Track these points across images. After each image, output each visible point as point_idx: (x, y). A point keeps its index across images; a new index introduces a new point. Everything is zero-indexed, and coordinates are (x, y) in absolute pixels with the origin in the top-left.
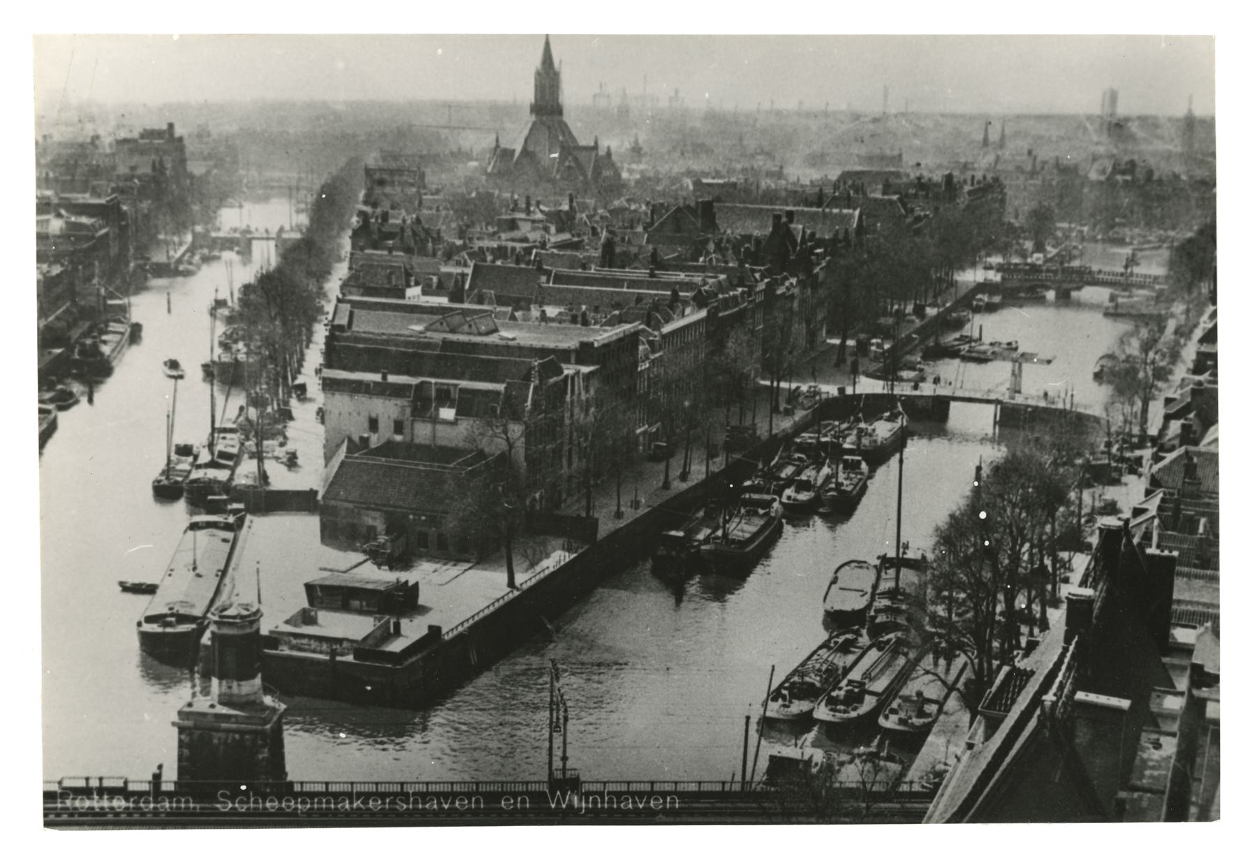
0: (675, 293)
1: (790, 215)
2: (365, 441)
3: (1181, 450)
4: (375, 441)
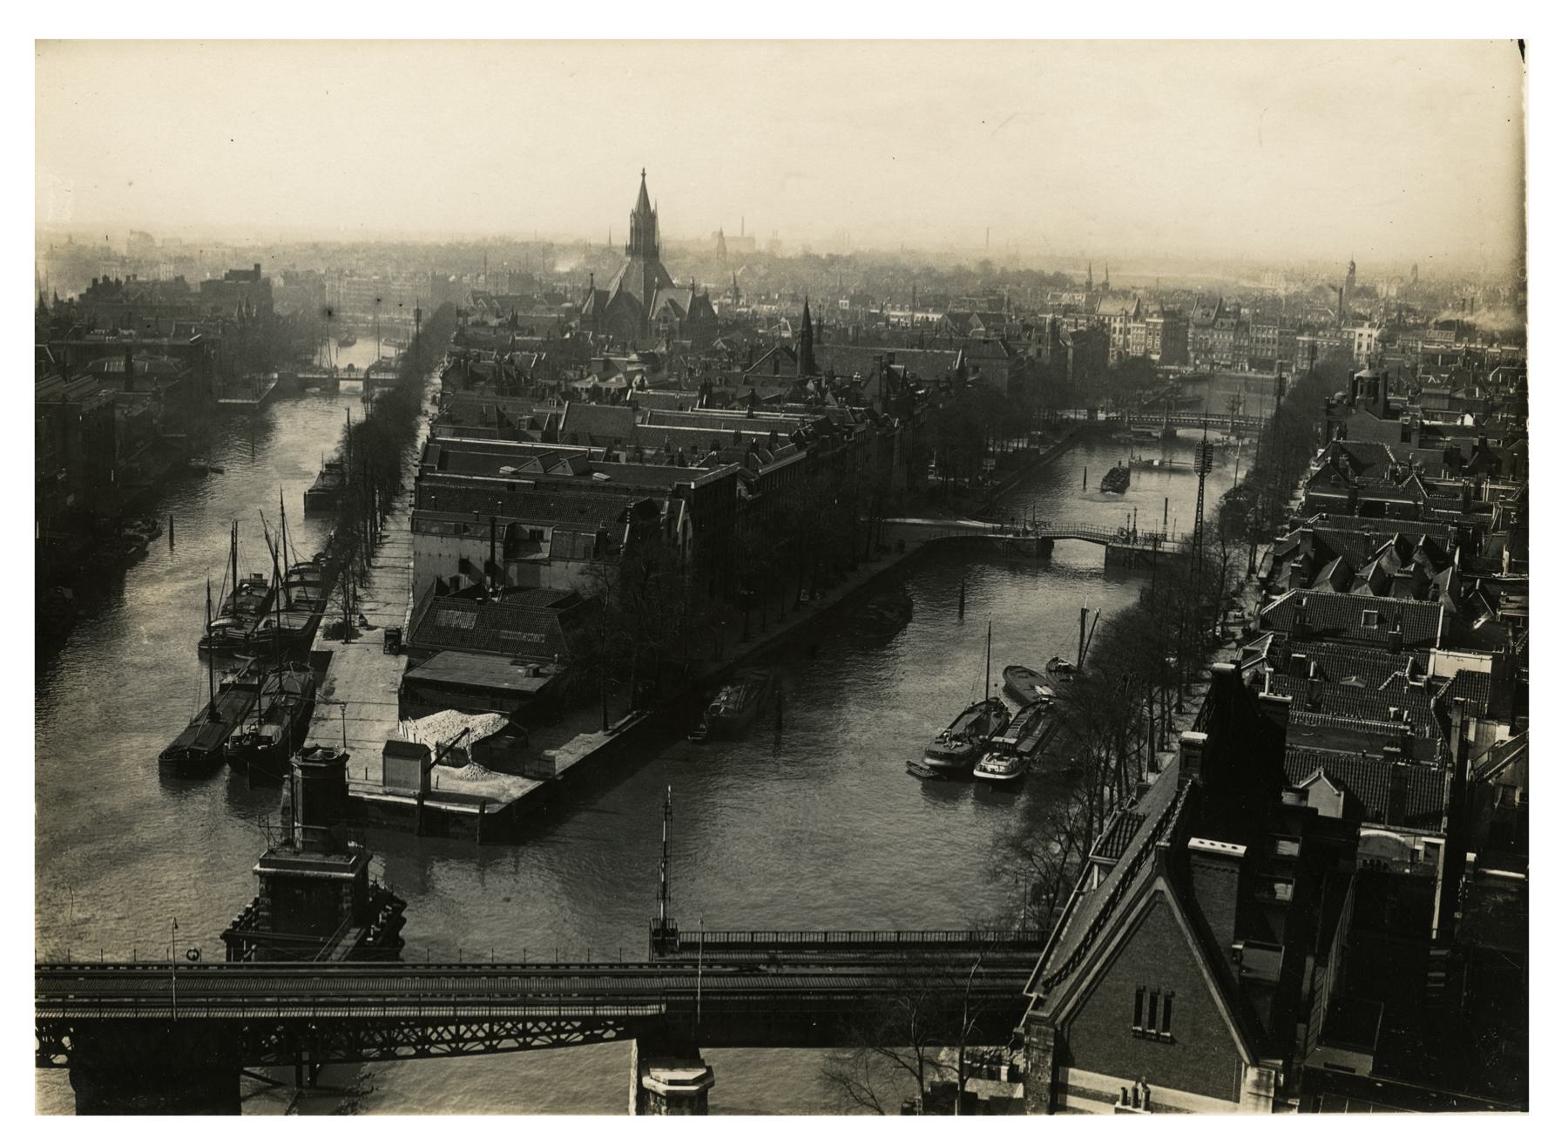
0: (774, 433)
1: (892, 355)
2: (455, 581)
3: (1293, 592)
4: (466, 582)
